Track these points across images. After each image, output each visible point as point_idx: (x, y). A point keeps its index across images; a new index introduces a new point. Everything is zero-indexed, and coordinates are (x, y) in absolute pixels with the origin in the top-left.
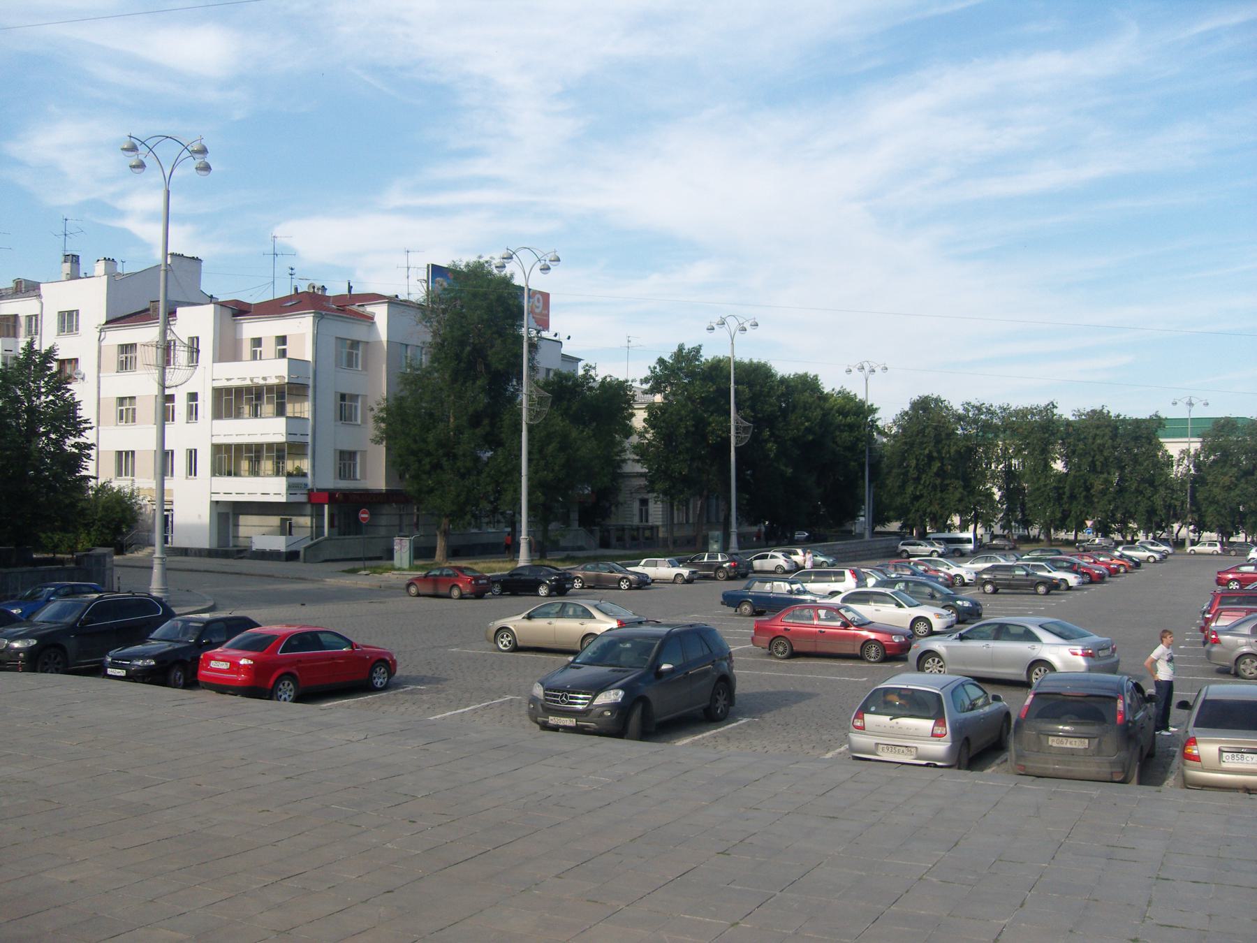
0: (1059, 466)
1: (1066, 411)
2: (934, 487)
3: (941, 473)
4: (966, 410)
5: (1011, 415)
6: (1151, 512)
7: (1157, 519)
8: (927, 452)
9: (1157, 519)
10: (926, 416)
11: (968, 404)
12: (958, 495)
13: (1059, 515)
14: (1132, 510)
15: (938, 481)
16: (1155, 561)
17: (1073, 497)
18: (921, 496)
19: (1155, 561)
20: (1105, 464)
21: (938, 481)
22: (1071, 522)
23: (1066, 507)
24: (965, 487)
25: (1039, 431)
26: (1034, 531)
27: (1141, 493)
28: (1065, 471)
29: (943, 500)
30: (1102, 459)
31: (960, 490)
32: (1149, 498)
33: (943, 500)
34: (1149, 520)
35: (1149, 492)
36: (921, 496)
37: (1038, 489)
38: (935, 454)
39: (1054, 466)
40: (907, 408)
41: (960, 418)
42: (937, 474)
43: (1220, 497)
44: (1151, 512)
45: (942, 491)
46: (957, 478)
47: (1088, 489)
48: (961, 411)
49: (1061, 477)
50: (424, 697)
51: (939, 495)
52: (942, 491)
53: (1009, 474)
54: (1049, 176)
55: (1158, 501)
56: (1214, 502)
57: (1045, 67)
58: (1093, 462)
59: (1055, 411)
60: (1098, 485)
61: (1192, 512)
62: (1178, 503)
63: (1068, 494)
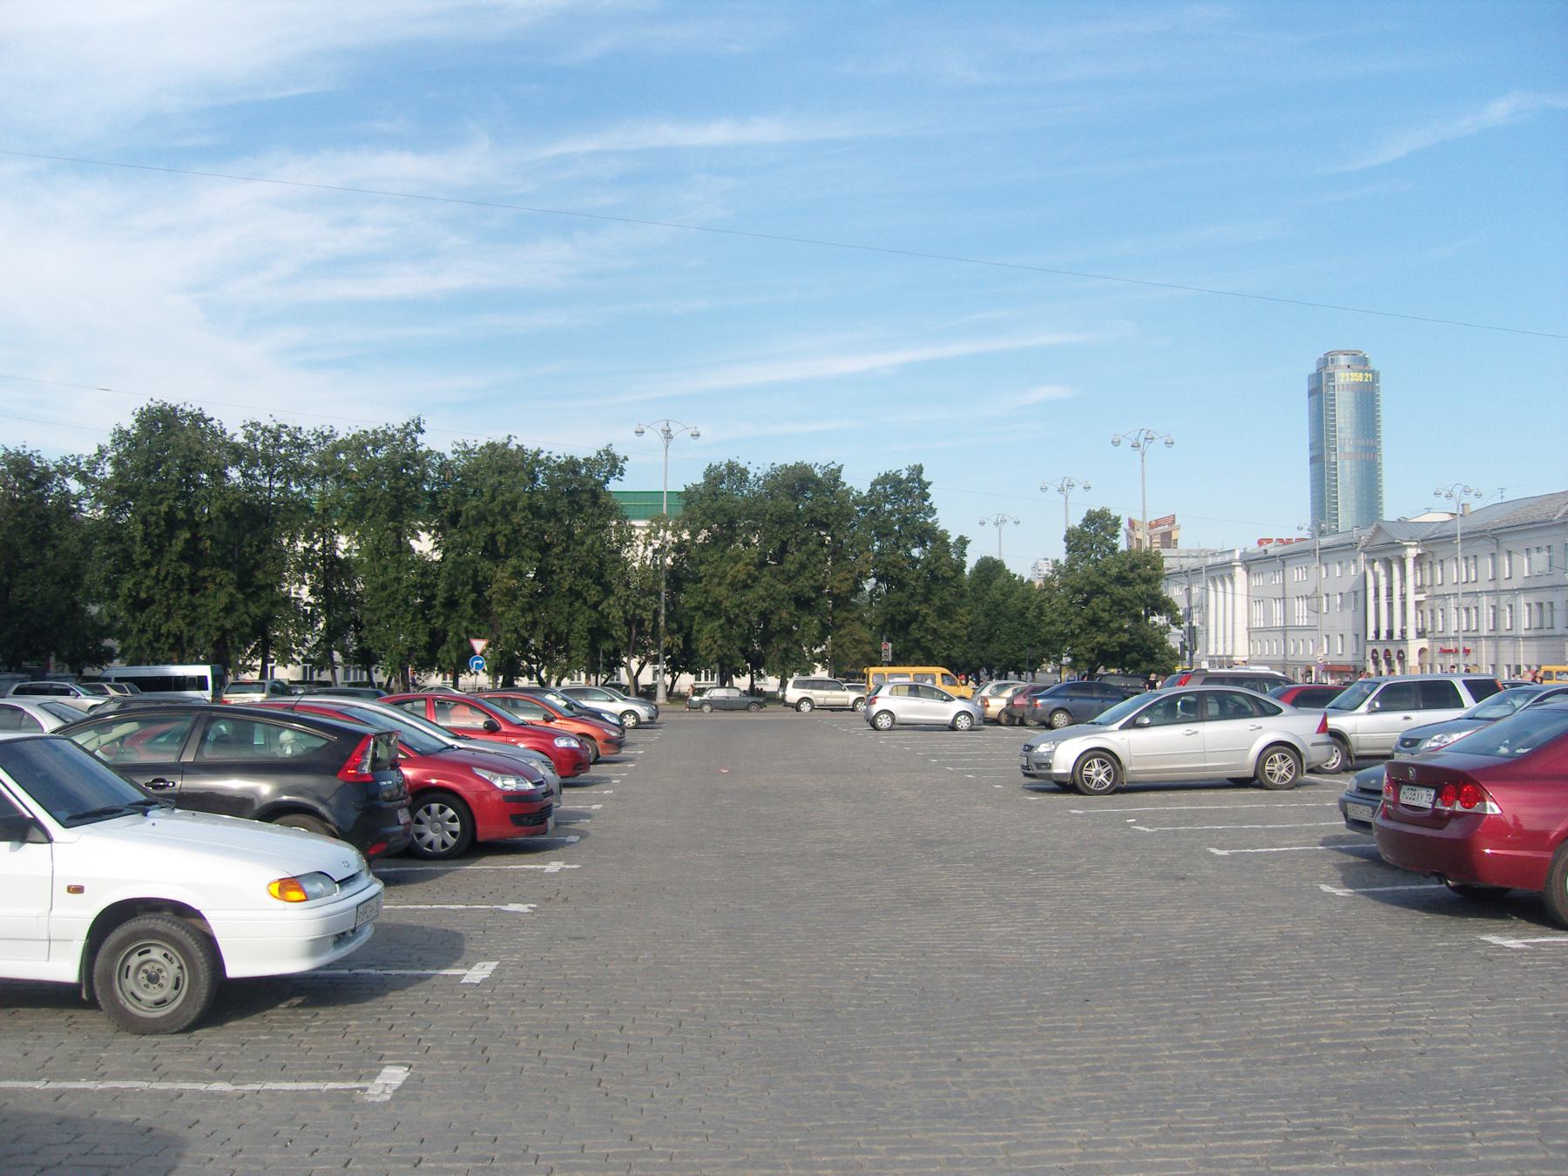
0: (424, 545)
1: (442, 440)
2: (178, 583)
3: (192, 554)
4: (251, 437)
5: (336, 449)
6: (598, 633)
7: (607, 646)
8: (164, 508)
9: (607, 646)
10: (167, 447)
11: (255, 425)
12: (223, 599)
13: (424, 639)
14: (563, 628)
15: (185, 570)
16: (639, 725)
17: (451, 604)
18: (150, 601)
19: (639, 725)
20: (512, 542)
21: (185, 570)
22: (448, 653)
23: (438, 623)
24: (240, 586)
25: (388, 483)
26: (380, 677)
27: (578, 595)
28: (437, 556)
29: (194, 608)
30: (507, 530)
31: (231, 590)
32: (595, 607)
33: (194, 608)
34: (593, 649)
35: (593, 594)
36: (150, 601)
37: (384, 587)
38: (181, 515)
39: (413, 543)
40: (129, 423)
41: (237, 454)
42: (183, 557)
43: (727, 604)
44: (598, 633)
45: (192, 592)
46: (228, 567)
47: (479, 588)
48: (240, 439)
49: (425, 567)
50: (695, 627)
51: (186, 597)
52: (192, 592)
53: (333, 570)
54: (403, 282)
55: (614, 610)
56: (713, 611)
57: (403, 167)
58: (492, 537)
59: (420, 438)
60: (502, 576)
61: (671, 633)
62: (648, 615)
63: (441, 596)
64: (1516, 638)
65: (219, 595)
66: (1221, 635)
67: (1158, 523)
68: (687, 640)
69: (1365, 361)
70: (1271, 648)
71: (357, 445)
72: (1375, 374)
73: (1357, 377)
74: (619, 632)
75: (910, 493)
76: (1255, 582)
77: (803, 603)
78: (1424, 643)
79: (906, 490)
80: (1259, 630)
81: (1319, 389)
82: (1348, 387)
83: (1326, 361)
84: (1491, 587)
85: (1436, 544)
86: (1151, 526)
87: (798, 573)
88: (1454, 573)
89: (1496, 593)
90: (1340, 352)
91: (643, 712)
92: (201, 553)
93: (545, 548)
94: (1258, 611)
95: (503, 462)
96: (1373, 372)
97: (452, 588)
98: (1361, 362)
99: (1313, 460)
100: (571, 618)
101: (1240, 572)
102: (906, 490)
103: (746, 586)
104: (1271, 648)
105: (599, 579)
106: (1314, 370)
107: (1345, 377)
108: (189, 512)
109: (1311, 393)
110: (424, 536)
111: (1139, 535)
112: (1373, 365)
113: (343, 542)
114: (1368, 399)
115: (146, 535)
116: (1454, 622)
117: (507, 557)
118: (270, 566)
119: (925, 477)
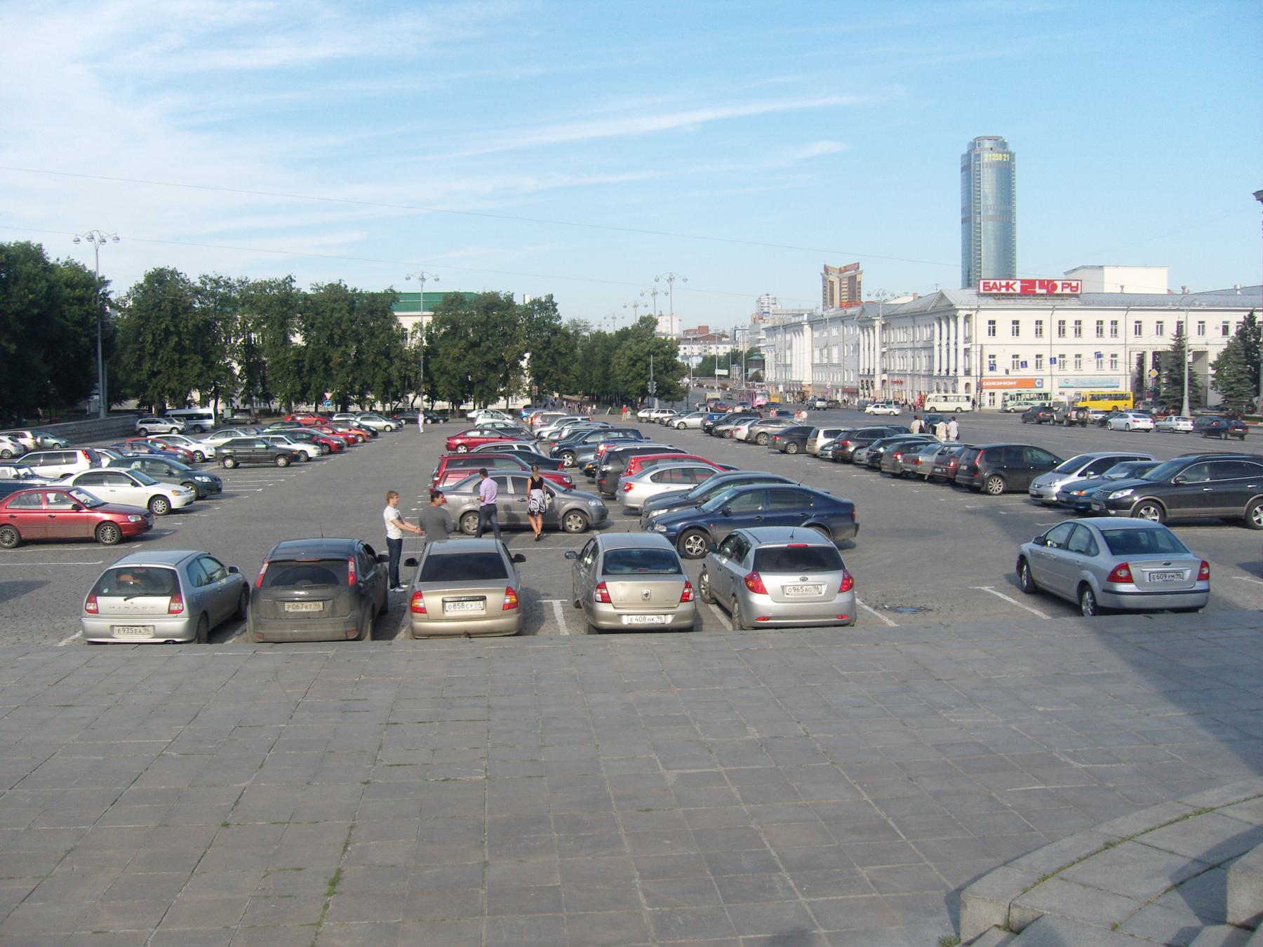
0: (298, 339)
1: (304, 285)
2: (173, 363)
3: (179, 348)
4: (204, 283)
5: (249, 288)
6: (388, 383)
8: (163, 326)
9: (392, 390)
12: (197, 371)
13: (299, 388)
15: (176, 357)
16: (392, 430)
17: (312, 370)
18: (159, 372)
20: (342, 338)
21: (176, 357)
22: (311, 394)
23: (306, 380)
24: (204, 362)
25: (278, 304)
26: (275, 405)
27: (377, 364)
28: (304, 344)
29: (182, 375)
32: (385, 370)
33: (182, 375)
34: (386, 391)
35: (385, 364)
36: (159, 372)
37: (278, 363)
38: (172, 329)
41: (197, 292)
42: (174, 349)
44: (388, 383)
46: (196, 353)
48: (198, 284)
49: (300, 351)
53: (249, 348)
56: (444, 372)
58: (331, 336)
59: (294, 285)
61: (425, 382)
64: (919, 376)
65: (195, 367)
66: (944, 342)
67: (846, 269)
68: (433, 386)
69: (1004, 145)
70: (849, 377)
71: (261, 287)
72: (1012, 155)
73: (998, 157)
74: (397, 383)
75: (547, 309)
76: (816, 334)
77: (491, 367)
78: (885, 377)
79: (547, 306)
80: (817, 365)
81: (969, 167)
82: (991, 165)
83: (975, 145)
84: (911, 345)
85: (894, 318)
86: (841, 271)
87: (487, 352)
88: (899, 336)
89: (914, 349)
90: (986, 138)
91: (393, 425)
92: (183, 347)
93: (360, 341)
94: (817, 353)
95: (336, 293)
96: (1010, 153)
97: (311, 362)
98: (1001, 145)
99: (963, 221)
100: (375, 375)
101: (807, 328)
102: (547, 306)
103: (459, 360)
104: (849, 377)
105: (387, 355)
106: (965, 151)
107: (988, 157)
108: (176, 326)
109: (963, 169)
110: (298, 335)
111: (831, 278)
112: (1011, 148)
113: (253, 336)
114: (1006, 173)
115: (154, 339)
116: (898, 364)
117: (339, 346)
118: (219, 353)
119: (555, 300)
